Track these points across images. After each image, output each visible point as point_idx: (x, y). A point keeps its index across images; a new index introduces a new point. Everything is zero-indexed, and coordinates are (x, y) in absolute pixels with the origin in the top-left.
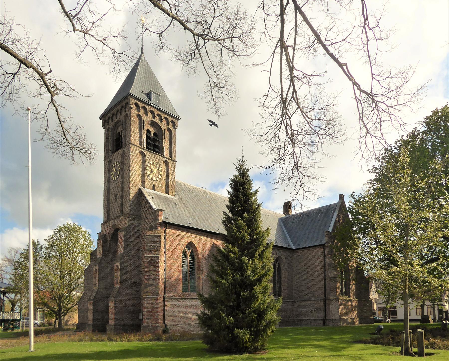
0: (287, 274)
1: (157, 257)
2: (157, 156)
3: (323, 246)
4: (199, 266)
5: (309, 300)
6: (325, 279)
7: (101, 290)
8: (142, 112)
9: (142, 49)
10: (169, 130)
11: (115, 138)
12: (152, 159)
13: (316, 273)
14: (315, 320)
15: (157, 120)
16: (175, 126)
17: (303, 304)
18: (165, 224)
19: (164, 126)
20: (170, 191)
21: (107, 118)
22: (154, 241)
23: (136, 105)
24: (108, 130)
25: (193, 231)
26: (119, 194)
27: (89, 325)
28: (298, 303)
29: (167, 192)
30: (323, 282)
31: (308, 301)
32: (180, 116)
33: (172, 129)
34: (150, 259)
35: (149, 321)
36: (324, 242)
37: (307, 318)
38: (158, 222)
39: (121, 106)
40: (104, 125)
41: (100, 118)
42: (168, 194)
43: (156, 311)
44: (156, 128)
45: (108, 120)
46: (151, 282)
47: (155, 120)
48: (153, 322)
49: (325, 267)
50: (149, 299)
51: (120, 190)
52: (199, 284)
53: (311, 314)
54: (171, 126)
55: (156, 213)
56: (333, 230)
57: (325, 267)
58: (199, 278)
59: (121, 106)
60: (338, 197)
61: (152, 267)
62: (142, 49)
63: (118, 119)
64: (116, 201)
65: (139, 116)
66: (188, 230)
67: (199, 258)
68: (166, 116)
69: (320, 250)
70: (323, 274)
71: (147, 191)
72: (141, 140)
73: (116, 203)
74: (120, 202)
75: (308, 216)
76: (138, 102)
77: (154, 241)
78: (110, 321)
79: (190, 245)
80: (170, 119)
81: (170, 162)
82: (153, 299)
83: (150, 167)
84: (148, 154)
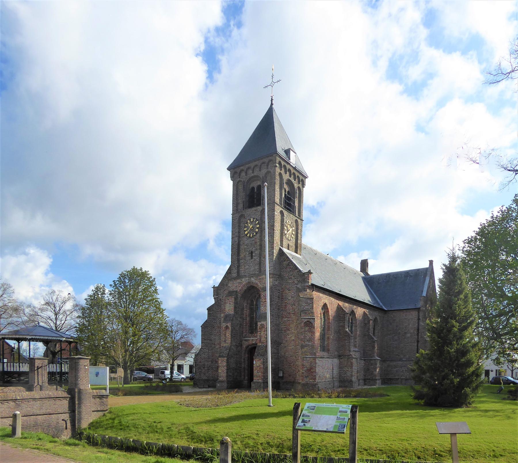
0: (380, 334)
1: (313, 319)
2: (292, 215)
3: (418, 309)
4: (329, 326)
5: (401, 360)
6: (418, 342)
7: (233, 347)
8: (283, 172)
9: (272, 100)
10: (299, 188)
11: (248, 193)
12: (289, 218)
13: (409, 335)
14: (406, 379)
15: (292, 179)
16: (303, 185)
17: (392, 364)
18: (314, 287)
19: (296, 185)
20: (299, 251)
21: (238, 170)
22: (307, 303)
23: (280, 163)
24: (238, 183)
25: (328, 293)
26: (257, 252)
27: (222, 382)
28: (388, 362)
29: (296, 252)
30: (416, 344)
31: (399, 361)
32: (308, 175)
33: (301, 187)
34: (306, 320)
35: (308, 379)
36: (418, 306)
37: (397, 377)
38: (307, 284)
39: (261, 161)
40: (233, 177)
41: (229, 169)
42: (297, 253)
43: (314, 370)
44: (290, 186)
45: (240, 172)
46: (307, 343)
47: (291, 179)
48: (311, 380)
49: (418, 330)
50: (308, 359)
51: (258, 247)
52: (328, 344)
53: (402, 373)
54: (300, 185)
55: (305, 276)
56: (427, 295)
57: (418, 330)
58: (328, 338)
59: (261, 161)
60: (429, 262)
61: (307, 328)
62: (272, 100)
63: (255, 174)
64: (252, 258)
65: (280, 174)
66: (325, 292)
67: (329, 319)
68: (299, 175)
69: (415, 314)
70: (416, 337)
71: (285, 250)
72: (280, 200)
73: (252, 260)
74: (258, 260)
75: (396, 278)
76: (281, 161)
77: (307, 303)
78: (254, 378)
79: (325, 306)
80: (301, 177)
81: (299, 220)
82: (312, 359)
83: (287, 227)
84: (286, 213)
